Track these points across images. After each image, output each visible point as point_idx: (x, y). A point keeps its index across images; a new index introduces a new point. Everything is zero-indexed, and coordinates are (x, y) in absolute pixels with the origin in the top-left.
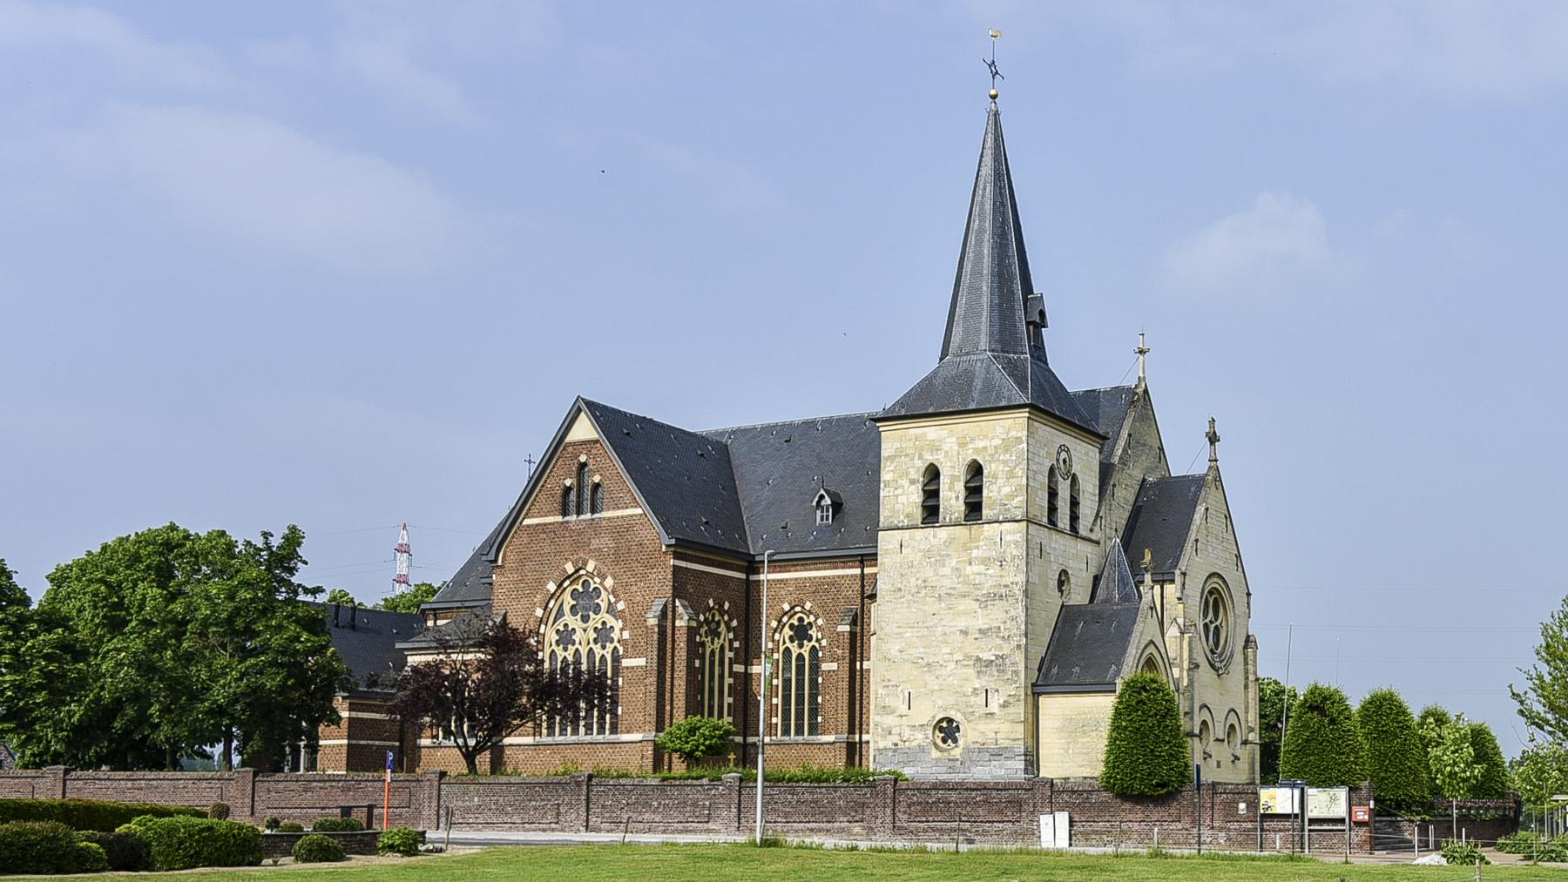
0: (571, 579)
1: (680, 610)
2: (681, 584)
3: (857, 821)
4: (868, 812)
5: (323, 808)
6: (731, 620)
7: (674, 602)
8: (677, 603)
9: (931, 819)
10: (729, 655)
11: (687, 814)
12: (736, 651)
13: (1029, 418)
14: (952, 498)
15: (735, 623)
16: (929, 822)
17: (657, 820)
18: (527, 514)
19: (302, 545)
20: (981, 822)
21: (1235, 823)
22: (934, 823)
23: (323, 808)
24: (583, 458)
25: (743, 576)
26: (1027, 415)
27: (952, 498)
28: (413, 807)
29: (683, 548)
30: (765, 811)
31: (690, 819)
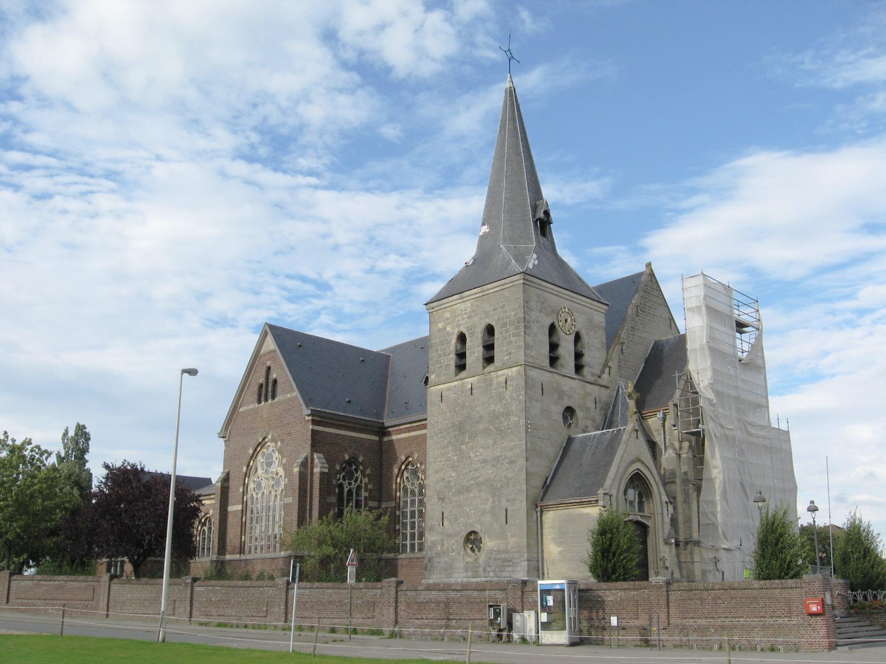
0: (398, 490)
1: (316, 461)
2: (317, 442)
3: (369, 618)
4: (377, 610)
5: (45, 600)
6: (365, 468)
7: (312, 455)
8: (315, 456)
9: (424, 616)
10: (364, 494)
11: (253, 610)
12: (370, 491)
13: (524, 283)
14: (475, 352)
15: (368, 471)
16: (423, 619)
17: (233, 614)
18: (241, 405)
19: (81, 424)
20: (465, 619)
21: (690, 620)
22: (427, 621)
23: (45, 600)
24: (268, 363)
25: (377, 438)
26: (522, 281)
27: (475, 352)
28: (95, 600)
29: (319, 418)
30: (172, 575)
31: (254, 614)
